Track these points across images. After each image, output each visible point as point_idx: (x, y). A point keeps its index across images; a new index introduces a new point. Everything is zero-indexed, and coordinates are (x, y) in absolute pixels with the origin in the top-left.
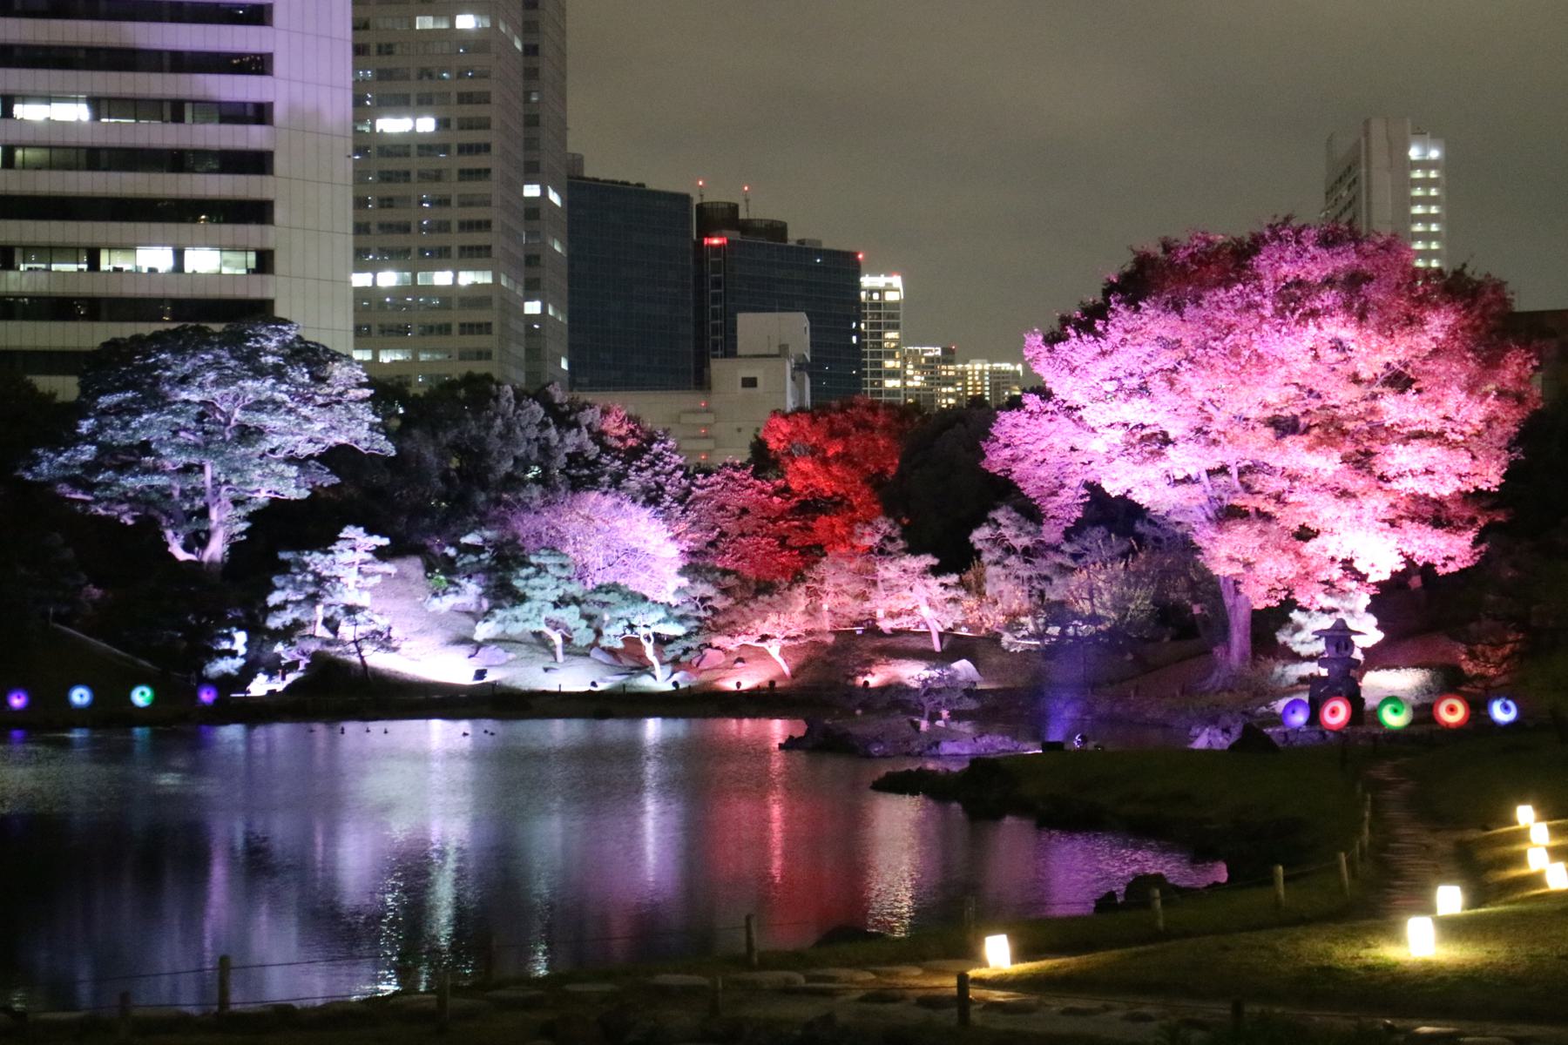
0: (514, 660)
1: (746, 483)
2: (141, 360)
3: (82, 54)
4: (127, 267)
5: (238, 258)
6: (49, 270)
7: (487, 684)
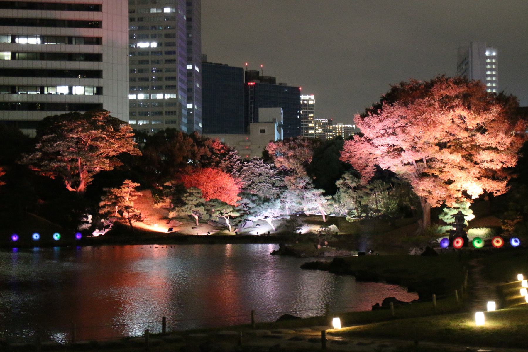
0: (182, 224)
1: (261, 165)
2: (56, 124)
3: (38, 21)
4: (53, 93)
5: (90, 89)
6: (27, 94)
7: (173, 232)
